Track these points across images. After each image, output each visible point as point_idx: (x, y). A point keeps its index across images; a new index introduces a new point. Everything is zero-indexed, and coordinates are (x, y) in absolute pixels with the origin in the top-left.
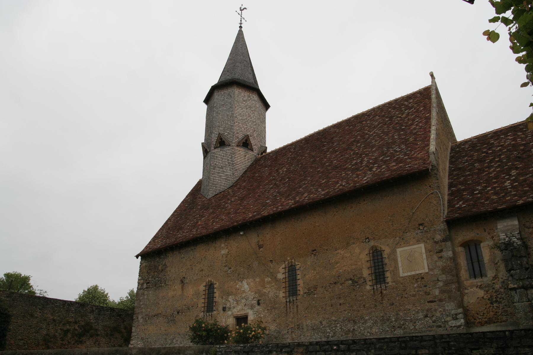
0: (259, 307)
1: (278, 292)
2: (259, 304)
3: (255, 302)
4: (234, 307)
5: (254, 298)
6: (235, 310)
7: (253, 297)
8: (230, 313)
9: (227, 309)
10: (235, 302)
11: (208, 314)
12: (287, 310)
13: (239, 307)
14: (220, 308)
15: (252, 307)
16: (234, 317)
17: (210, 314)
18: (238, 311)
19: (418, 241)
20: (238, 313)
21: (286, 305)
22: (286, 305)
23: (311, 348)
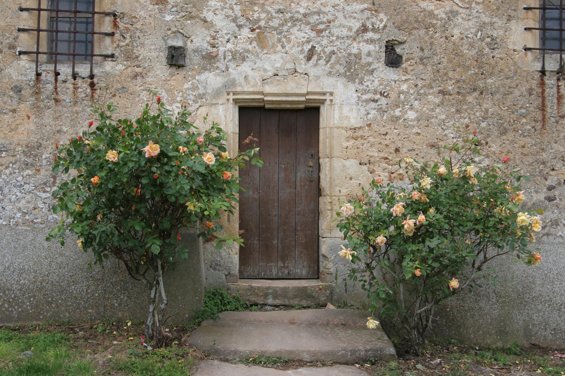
0: (391, 74)
1: (499, 22)
2: (393, 60)
3: (370, 49)
4: (239, 57)
5: (364, 29)
6: (245, 67)
7: (356, 25)
8: (212, 80)
9: (193, 60)
10: (246, 32)
11: (65, 70)
12: (543, 108)
13: (273, 61)
14: (152, 51)
15: (353, 69)
16: (236, 101)
17: (83, 70)
18: (271, 76)
19: (395, 346)
20: (268, 89)
21: (542, 84)
22: (542, 84)
23: (89, 45)
